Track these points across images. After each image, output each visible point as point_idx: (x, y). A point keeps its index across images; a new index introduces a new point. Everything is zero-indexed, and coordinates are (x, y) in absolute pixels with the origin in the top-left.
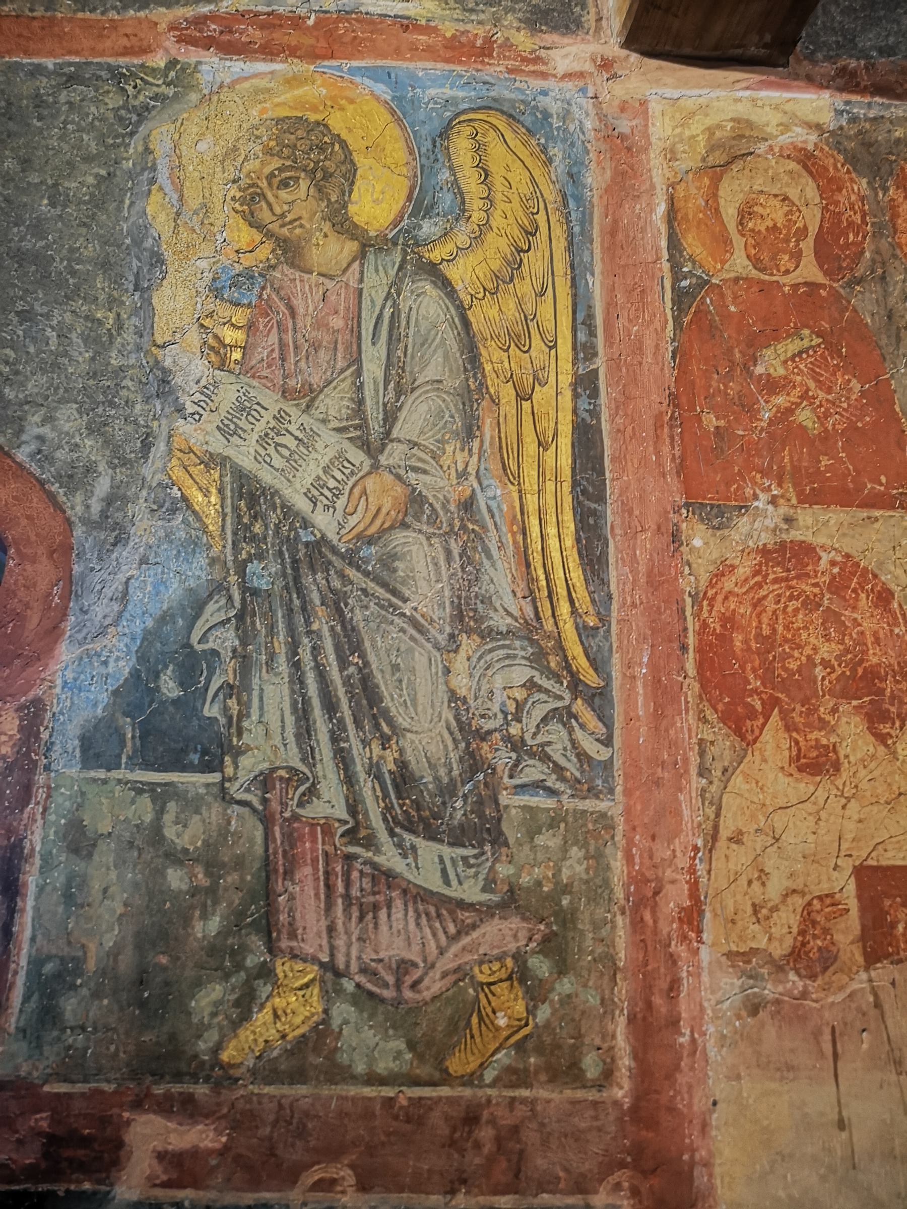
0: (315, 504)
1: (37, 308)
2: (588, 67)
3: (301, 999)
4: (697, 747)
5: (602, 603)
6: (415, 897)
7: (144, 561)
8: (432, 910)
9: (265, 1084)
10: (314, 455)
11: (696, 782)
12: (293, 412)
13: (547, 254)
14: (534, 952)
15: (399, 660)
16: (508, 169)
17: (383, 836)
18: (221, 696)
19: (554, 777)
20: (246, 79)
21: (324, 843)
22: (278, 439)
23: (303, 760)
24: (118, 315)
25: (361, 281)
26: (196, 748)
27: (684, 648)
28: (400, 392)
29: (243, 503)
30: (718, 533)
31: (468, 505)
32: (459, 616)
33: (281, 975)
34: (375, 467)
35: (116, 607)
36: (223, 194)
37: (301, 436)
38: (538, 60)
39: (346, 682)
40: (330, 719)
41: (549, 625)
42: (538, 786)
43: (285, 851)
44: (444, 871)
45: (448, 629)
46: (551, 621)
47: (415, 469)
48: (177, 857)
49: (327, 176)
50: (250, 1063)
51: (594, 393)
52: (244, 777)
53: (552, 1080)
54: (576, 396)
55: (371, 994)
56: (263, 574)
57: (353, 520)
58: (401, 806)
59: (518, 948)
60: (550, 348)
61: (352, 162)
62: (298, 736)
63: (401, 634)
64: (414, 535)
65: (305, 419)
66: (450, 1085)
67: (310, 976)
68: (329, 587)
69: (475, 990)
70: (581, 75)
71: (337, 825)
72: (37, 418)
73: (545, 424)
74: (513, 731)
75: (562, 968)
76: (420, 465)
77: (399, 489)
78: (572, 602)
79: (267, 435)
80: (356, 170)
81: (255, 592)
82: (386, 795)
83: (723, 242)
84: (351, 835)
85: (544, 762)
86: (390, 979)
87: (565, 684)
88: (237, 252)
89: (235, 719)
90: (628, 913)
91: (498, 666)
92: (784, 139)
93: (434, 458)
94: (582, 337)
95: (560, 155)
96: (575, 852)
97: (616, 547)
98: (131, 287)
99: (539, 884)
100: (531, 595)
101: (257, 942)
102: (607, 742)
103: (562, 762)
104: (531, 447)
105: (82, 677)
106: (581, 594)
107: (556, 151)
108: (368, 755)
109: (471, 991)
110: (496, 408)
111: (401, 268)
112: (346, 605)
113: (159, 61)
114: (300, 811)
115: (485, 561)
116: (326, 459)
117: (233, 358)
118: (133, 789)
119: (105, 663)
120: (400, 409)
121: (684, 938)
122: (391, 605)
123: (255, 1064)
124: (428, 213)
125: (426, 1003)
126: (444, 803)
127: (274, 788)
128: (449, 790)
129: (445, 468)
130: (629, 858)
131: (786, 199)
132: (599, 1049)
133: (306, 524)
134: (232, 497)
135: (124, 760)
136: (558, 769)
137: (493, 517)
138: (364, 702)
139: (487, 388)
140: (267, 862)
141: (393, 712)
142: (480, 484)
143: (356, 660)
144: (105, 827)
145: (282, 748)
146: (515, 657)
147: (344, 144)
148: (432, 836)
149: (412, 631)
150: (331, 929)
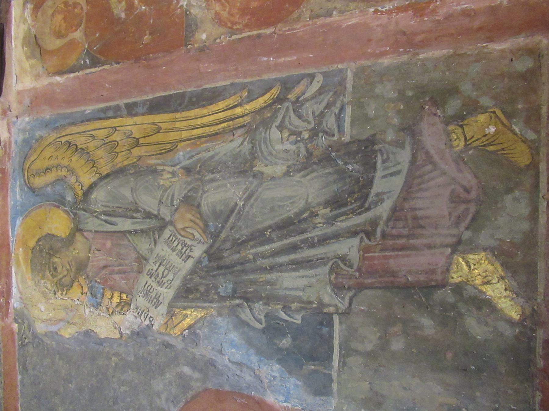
0: (190, 256)
1: (111, 394)
2: (5, 122)
3: (476, 267)
4: (314, 20)
5: (235, 88)
6: (408, 192)
7: (221, 352)
8: (417, 181)
9: (537, 291)
10: (167, 257)
11: (336, 17)
12: (148, 268)
13: (78, 135)
14: (443, 112)
15: (268, 207)
16: (45, 158)
17: (370, 215)
18: (290, 313)
19: (333, 108)
20: (18, 286)
21: (375, 252)
22: (160, 275)
23: (325, 264)
24: (113, 355)
25: (91, 231)
26: (319, 329)
27: (259, 36)
28: (137, 211)
29: (190, 297)
30: (199, 24)
31: (188, 170)
32: (243, 173)
33: (460, 279)
34: (171, 223)
35: (245, 369)
36: (60, 300)
37: (158, 264)
38: (5, 146)
39: (281, 238)
40: (301, 248)
41: (248, 119)
42: (339, 118)
43: (380, 276)
44: (392, 175)
45: (251, 179)
46: (246, 118)
47: (172, 201)
48: (384, 342)
49: (51, 248)
50: (521, 300)
51: (135, 104)
52: (337, 301)
53: (534, 91)
54: (136, 115)
55: (474, 219)
56: (225, 286)
57: (197, 235)
58: (352, 203)
59: (441, 122)
60: (116, 130)
61: (46, 236)
62: (312, 267)
63: (254, 207)
64: (203, 200)
65: (151, 261)
66: (538, 164)
67: (461, 260)
68: (230, 249)
69: (470, 149)
70: (8, 124)
71: (363, 244)
72: (158, 401)
73: (149, 130)
74: (306, 136)
75: (454, 91)
76: (170, 199)
77: (182, 209)
78: (235, 107)
79: (158, 282)
80: (49, 234)
81: (235, 291)
82: (345, 214)
83: (72, 44)
84: (369, 235)
85: (324, 115)
86: (463, 207)
87: (279, 106)
88: (82, 294)
89: (302, 305)
90: (417, 51)
91: (270, 148)
92: (29, 20)
93: (166, 191)
94: (110, 114)
95: (39, 132)
96: (378, 90)
97: (207, 83)
98: (101, 347)
99: (399, 112)
100: (232, 131)
101: (439, 295)
102: (312, 77)
103: (324, 104)
104: (159, 137)
105: (282, 391)
106: (231, 101)
107: (38, 134)
108: (321, 225)
109: (470, 152)
110: (143, 158)
111: (86, 211)
112: (239, 239)
113: (15, 326)
114: (355, 267)
115: (215, 159)
116: (169, 250)
117: (125, 298)
118: (343, 367)
119: (274, 377)
120: (144, 210)
121: (434, 11)
122: (239, 213)
123: (523, 298)
124: (64, 198)
125: (479, 182)
126: (350, 177)
127: (342, 282)
128: (342, 174)
129: (171, 184)
130: (383, 54)
131: (53, 15)
132: (512, 60)
133: (199, 261)
134: (188, 302)
135: (326, 372)
136: (328, 106)
137: (193, 156)
138: (291, 228)
139: (134, 163)
140: (387, 287)
141: (296, 210)
142: (178, 164)
143: (268, 233)
144: (365, 386)
145: (319, 277)
146: (265, 138)
147: (39, 240)
148: (370, 183)
149: (252, 200)
150: (430, 247)
